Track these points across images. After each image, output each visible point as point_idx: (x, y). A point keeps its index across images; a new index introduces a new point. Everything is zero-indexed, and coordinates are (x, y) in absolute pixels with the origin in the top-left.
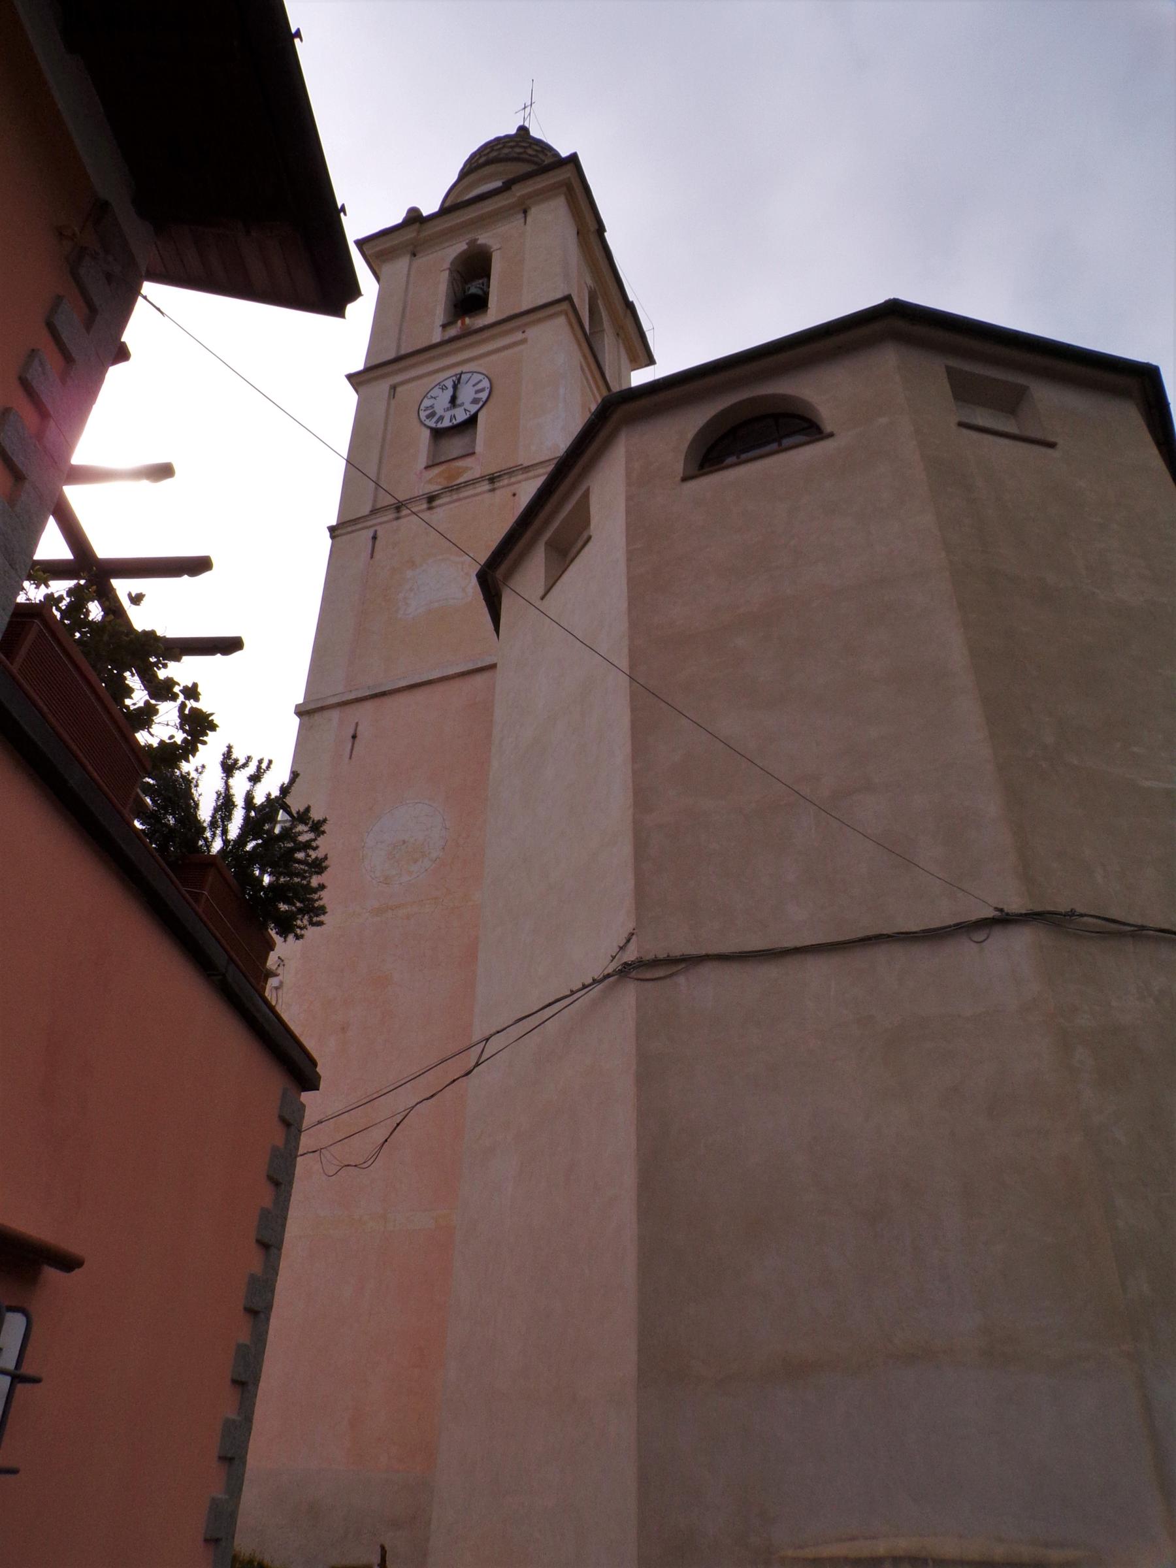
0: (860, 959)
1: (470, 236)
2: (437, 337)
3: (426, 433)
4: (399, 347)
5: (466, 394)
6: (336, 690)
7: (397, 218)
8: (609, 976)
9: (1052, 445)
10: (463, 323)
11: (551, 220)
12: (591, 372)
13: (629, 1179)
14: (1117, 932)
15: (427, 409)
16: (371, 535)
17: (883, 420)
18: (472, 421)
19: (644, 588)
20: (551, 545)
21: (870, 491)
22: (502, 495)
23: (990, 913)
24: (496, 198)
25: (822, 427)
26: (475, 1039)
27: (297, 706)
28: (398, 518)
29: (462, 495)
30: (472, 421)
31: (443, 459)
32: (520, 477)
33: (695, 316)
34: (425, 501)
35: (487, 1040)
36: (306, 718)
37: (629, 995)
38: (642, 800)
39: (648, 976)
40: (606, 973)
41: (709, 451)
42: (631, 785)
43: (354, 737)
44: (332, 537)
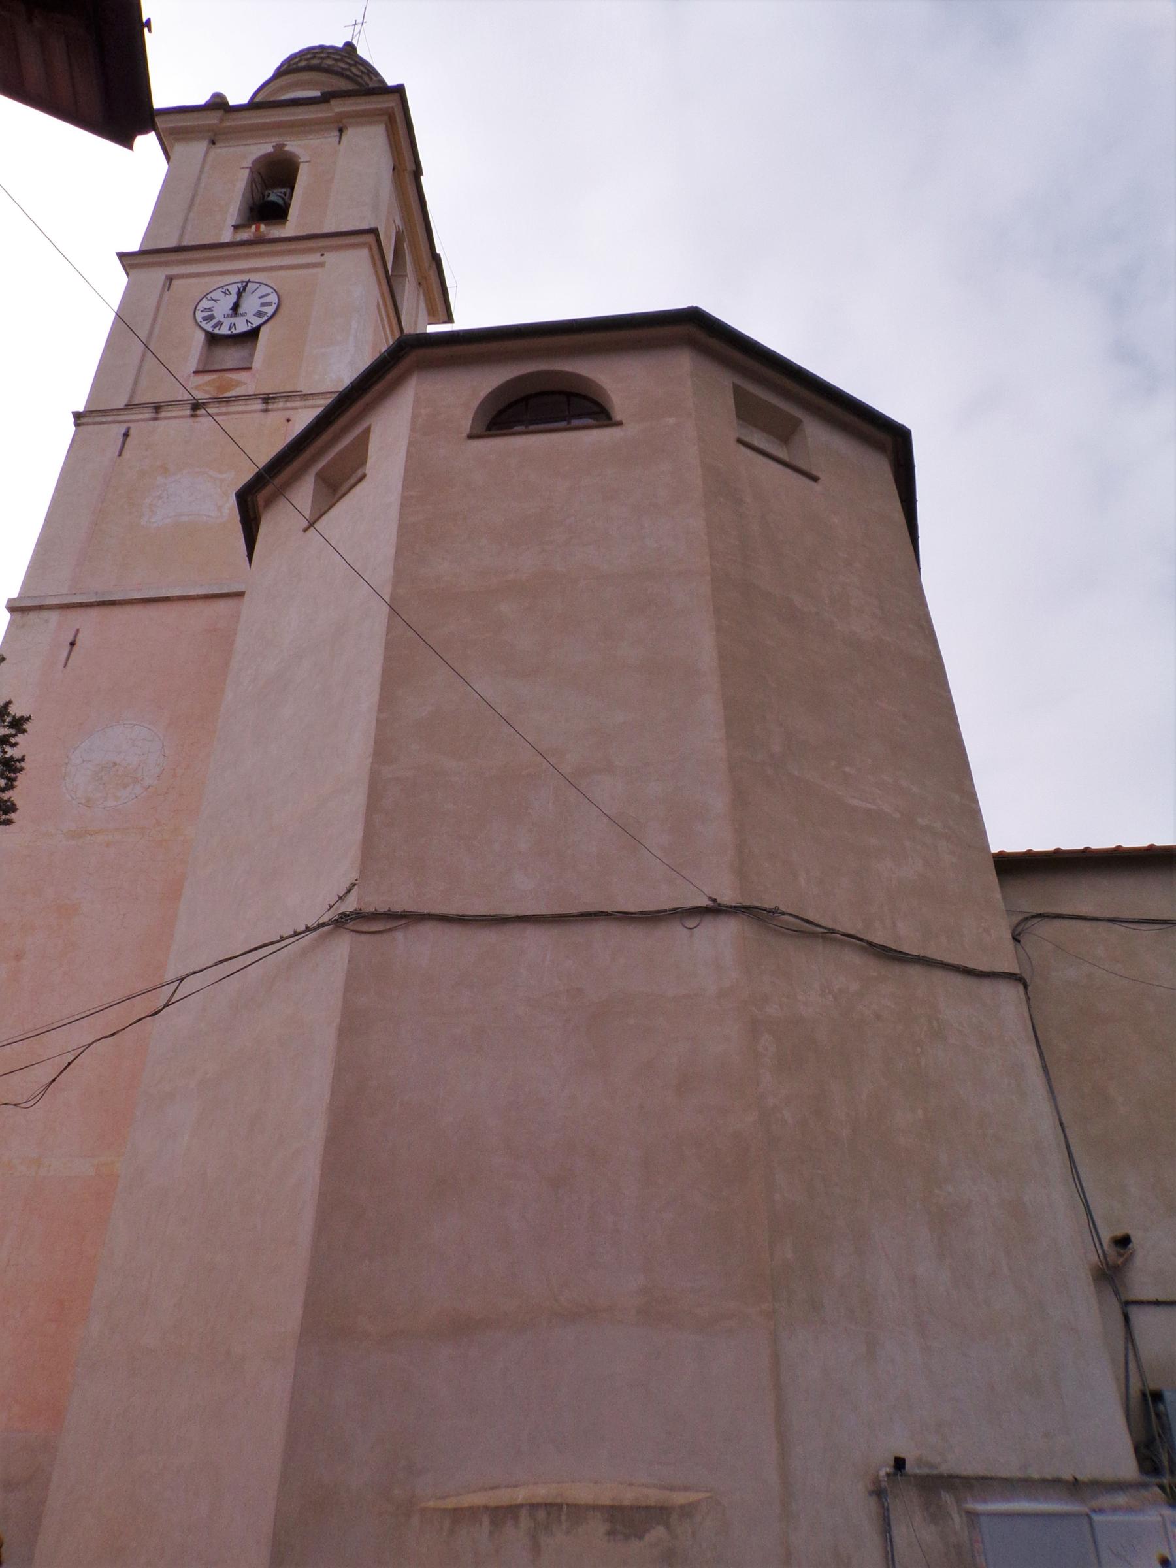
0: (578, 933)
1: (277, 140)
2: (227, 236)
3: (201, 336)
4: (182, 235)
5: (250, 304)
6: (58, 589)
7: (201, 99)
8: (323, 925)
9: (815, 479)
10: (258, 229)
11: (366, 146)
12: (387, 311)
13: (317, 1132)
14: (812, 932)
15: (204, 310)
16: (123, 431)
17: (671, 421)
18: (252, 335)
19: (414, 540)
20: (321, 477)
21: (645, 486)
22: (275, 418)
23: (704, 902)
24: (312, 108)
25: (613, 415)
26: (167, 979)
27: (10, 601)
28: (156, 419)
29: (232, 409)
30: (252, 335)
31: (217, 367)
32: (297, 404)
33: (504, 271)
34: (189, 407)
35: (182, 980)
36: (18, 615)
37: (342, 946)
38: (382, 752)
39: (365, 928)
40: (321, 921)
41: (501, 413)
42: (373, 735)
43: (72, 644)
44: (77, 424)
